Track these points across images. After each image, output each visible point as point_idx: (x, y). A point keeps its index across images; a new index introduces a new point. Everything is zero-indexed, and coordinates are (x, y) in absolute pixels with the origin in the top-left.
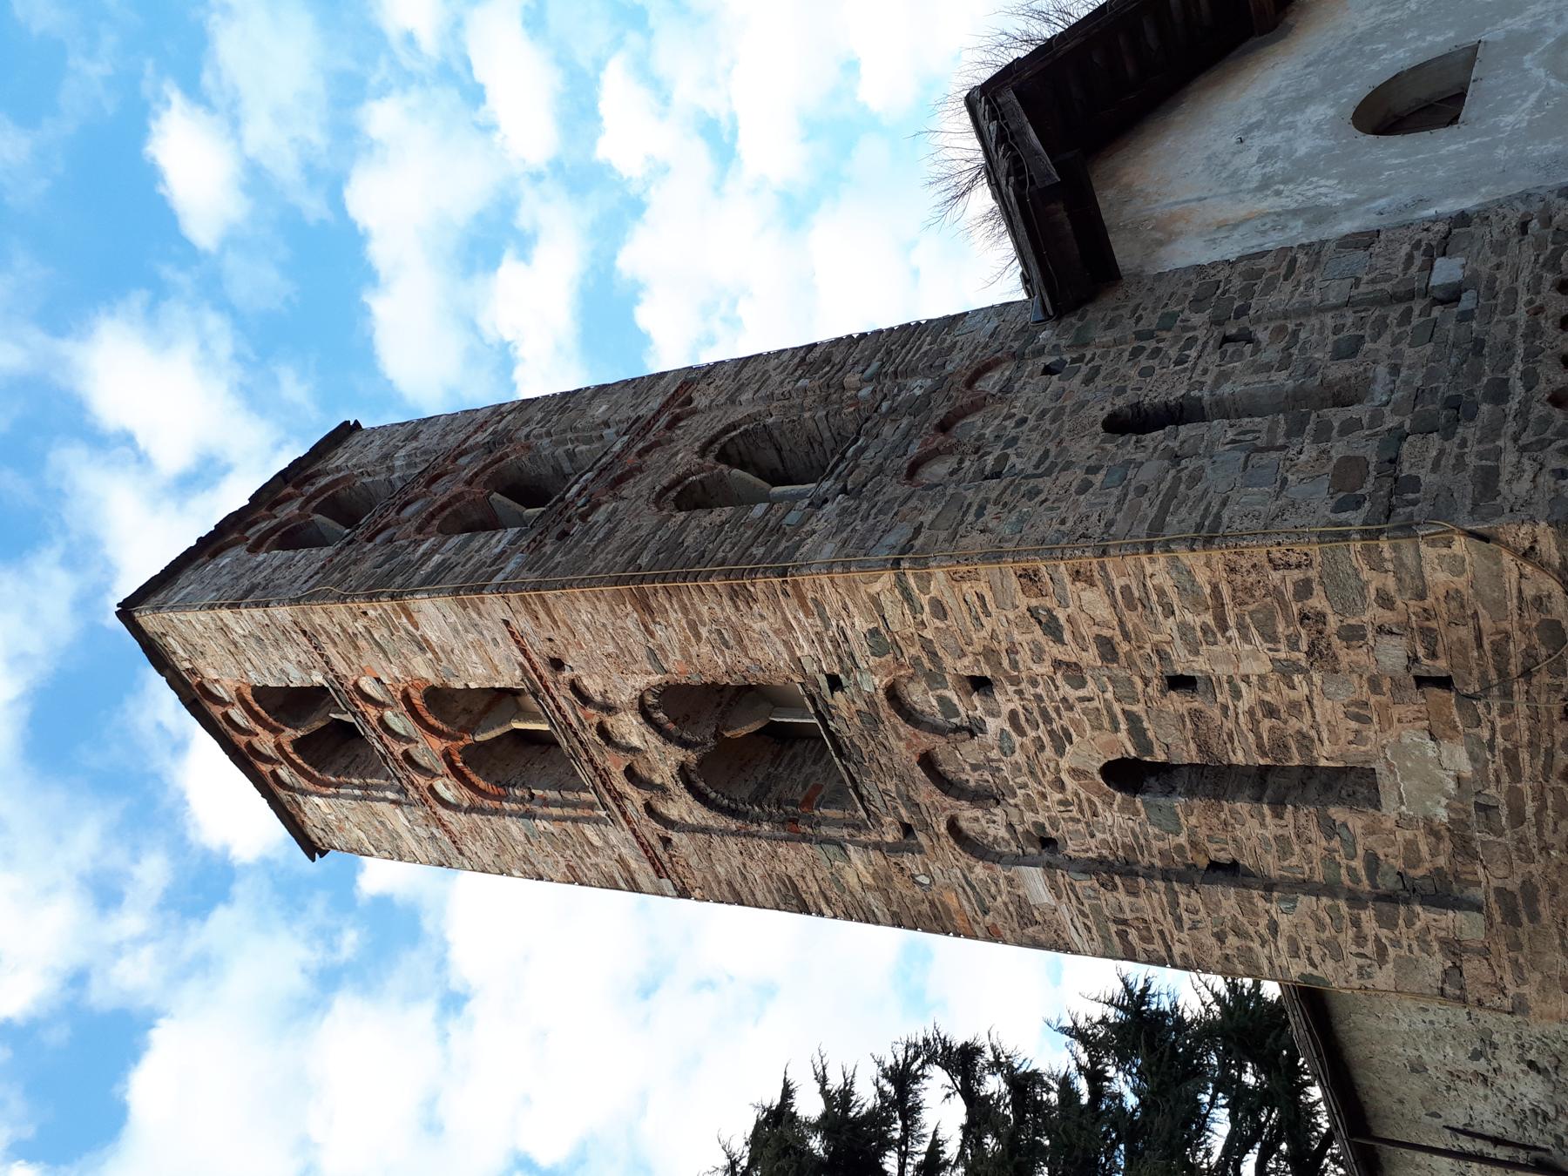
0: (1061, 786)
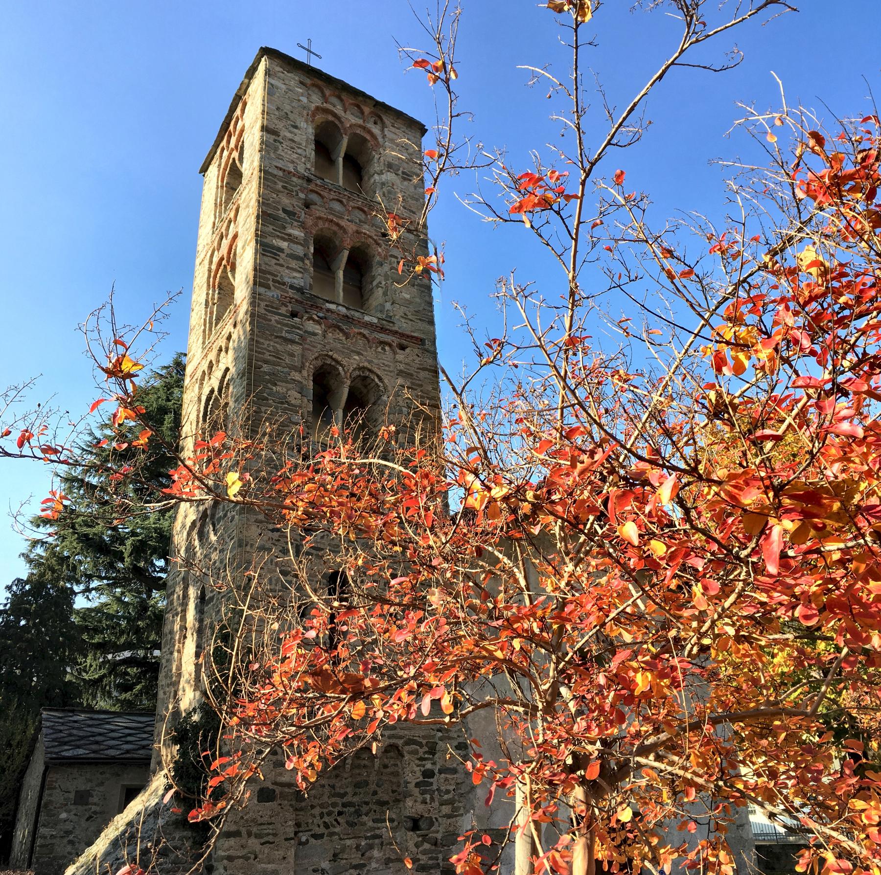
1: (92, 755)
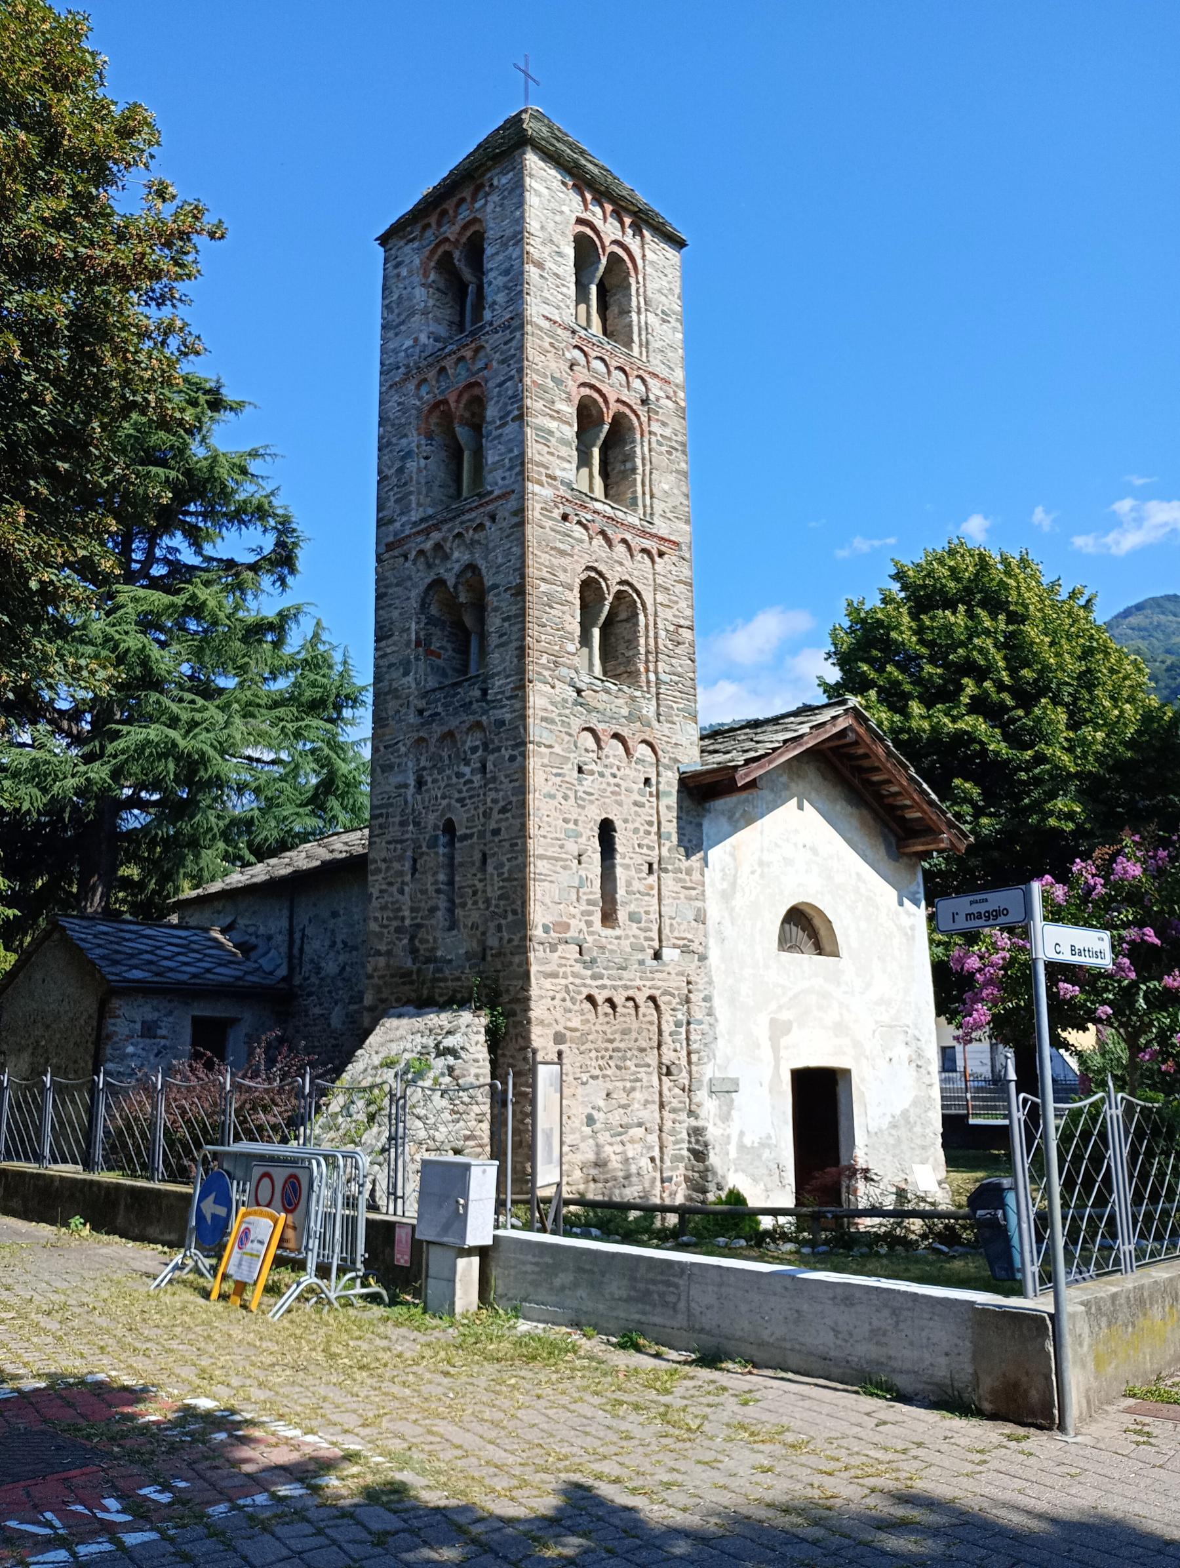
0: (443, 797)
1: (156, 979)
